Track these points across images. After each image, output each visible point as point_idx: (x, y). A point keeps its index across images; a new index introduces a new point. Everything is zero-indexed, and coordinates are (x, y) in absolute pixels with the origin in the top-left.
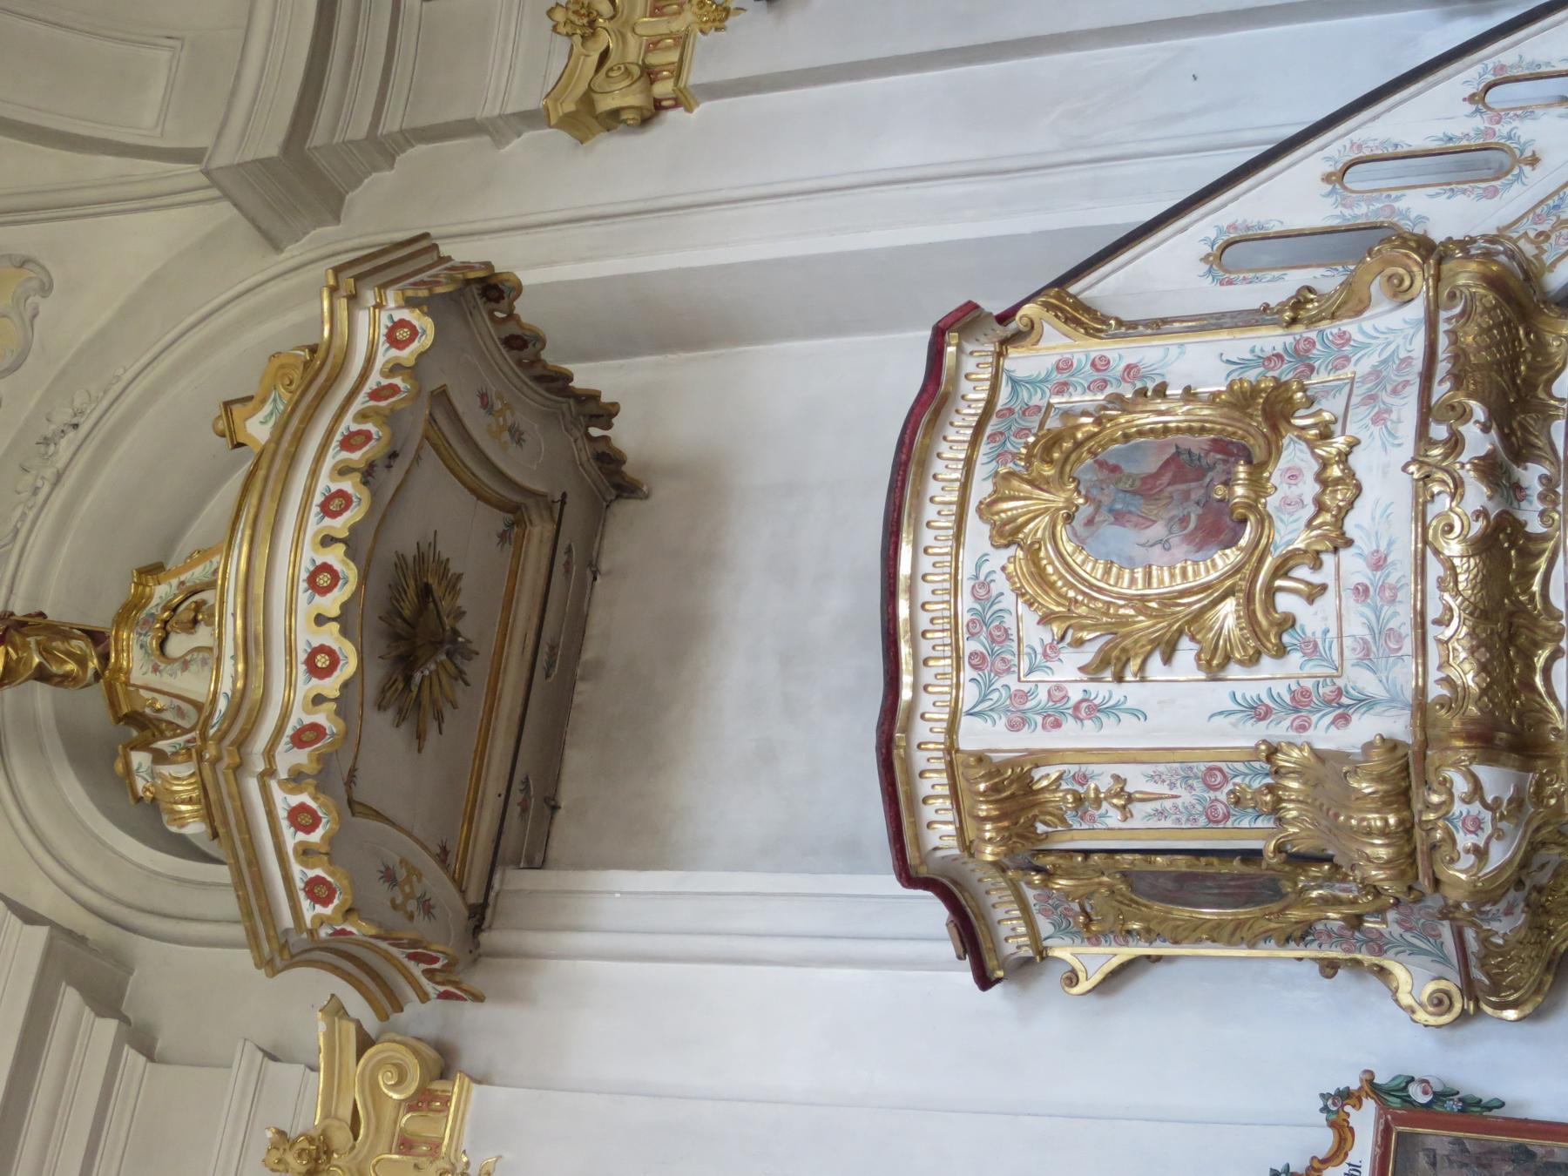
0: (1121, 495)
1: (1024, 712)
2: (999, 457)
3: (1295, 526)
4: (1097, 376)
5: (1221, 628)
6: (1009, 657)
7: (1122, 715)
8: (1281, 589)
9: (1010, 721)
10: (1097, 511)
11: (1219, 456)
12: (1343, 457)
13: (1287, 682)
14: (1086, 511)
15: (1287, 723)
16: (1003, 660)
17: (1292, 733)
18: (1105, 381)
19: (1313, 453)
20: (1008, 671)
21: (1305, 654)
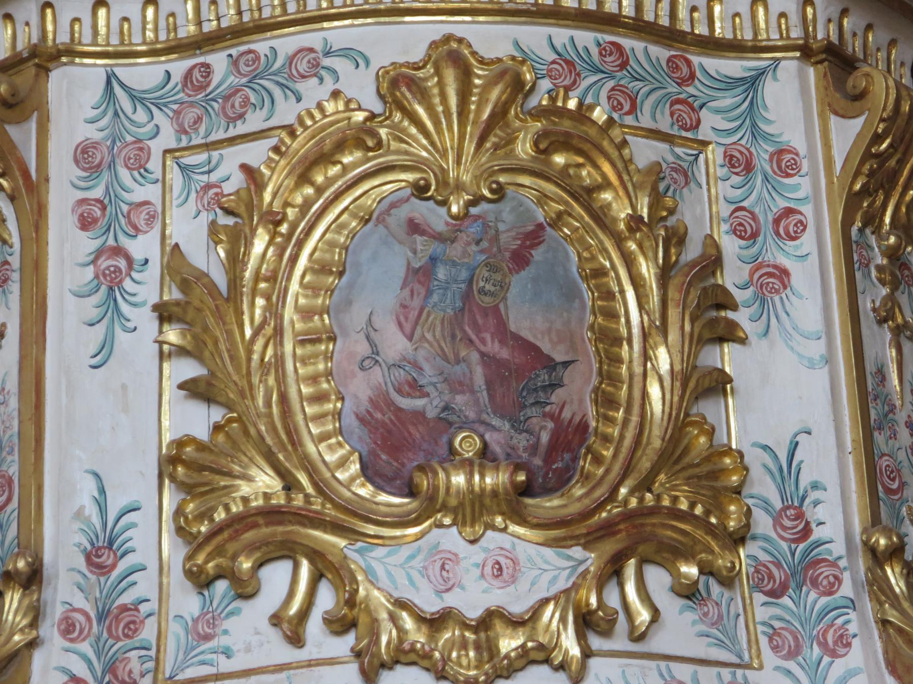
0: (464, 274)
1: (112, 165)
2: (568, 66)
3: (403, 581)
4: (766, 220)
5: (230, 474)
6: (202, 130)
7: (101, 329)
8: (296, 567)
9: (95, 145)
10: (439, 237)
11: (545, 438)
12: (541, 655)
13: (154, 596)
14: (436, 217)
15: (80, 601)
16: (199, 120)
17: (59, 611)
18: (754, 236)
19: (545, 602)
20: (182, 131)
21: (195, 621)
